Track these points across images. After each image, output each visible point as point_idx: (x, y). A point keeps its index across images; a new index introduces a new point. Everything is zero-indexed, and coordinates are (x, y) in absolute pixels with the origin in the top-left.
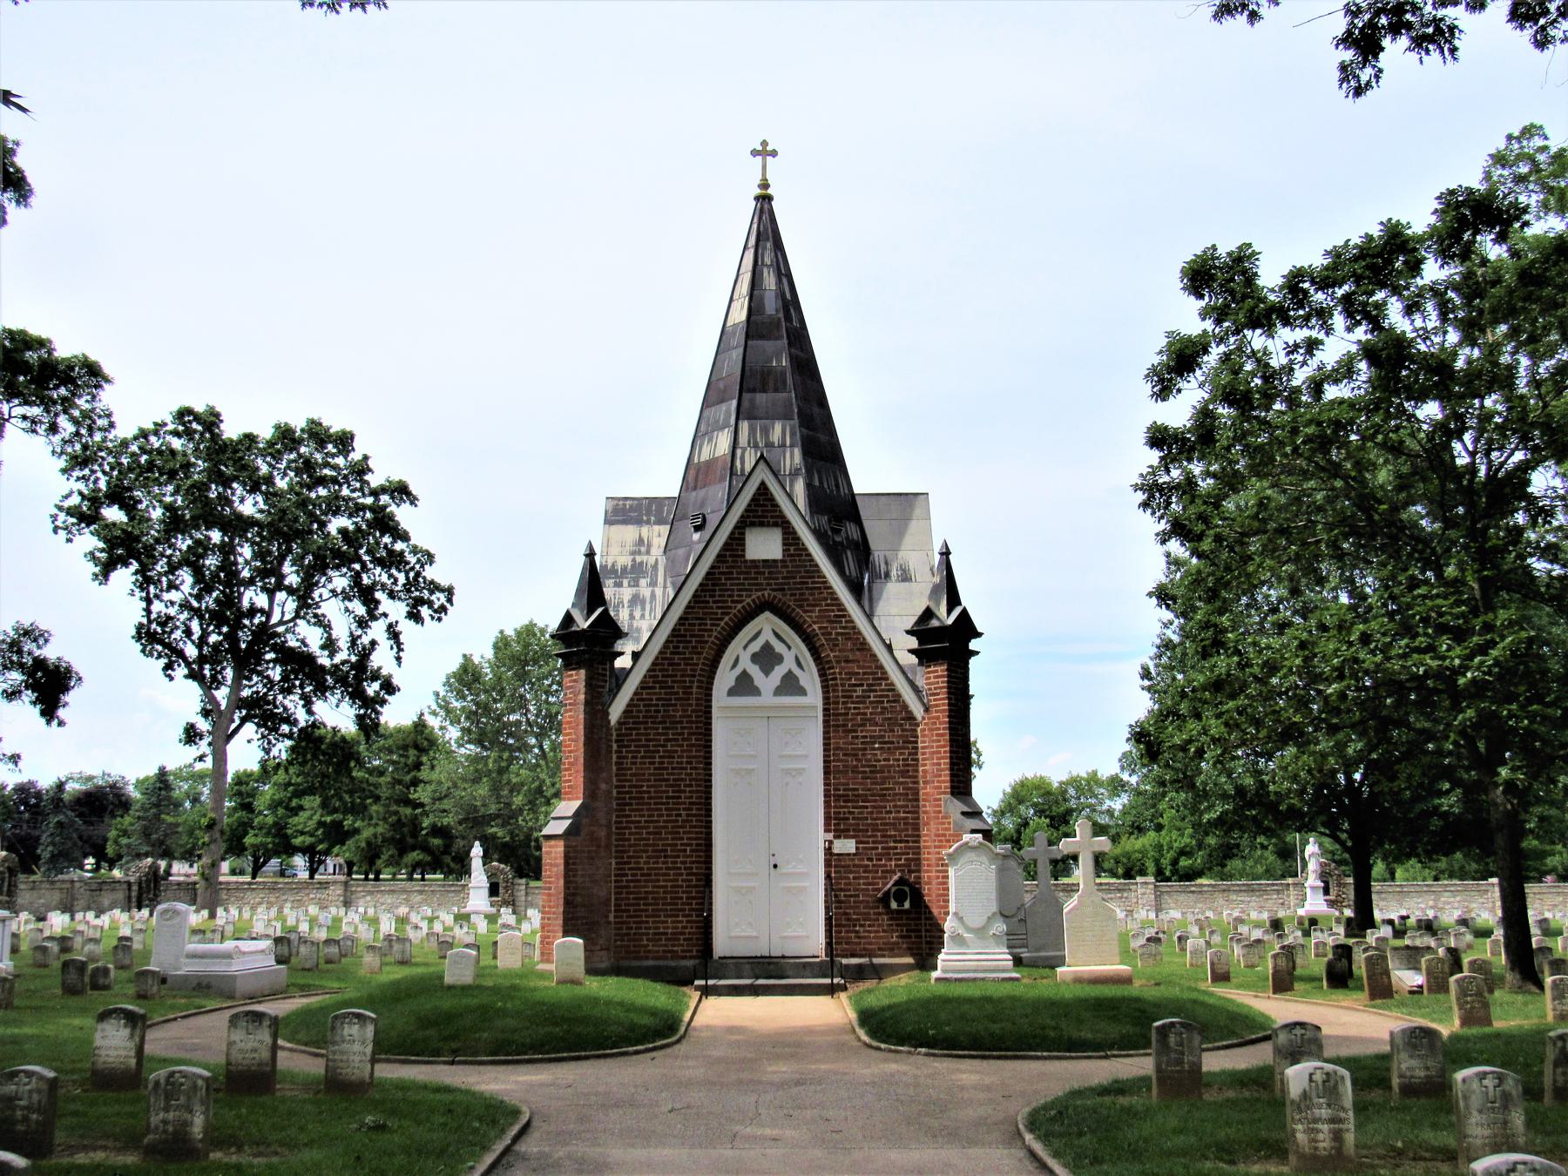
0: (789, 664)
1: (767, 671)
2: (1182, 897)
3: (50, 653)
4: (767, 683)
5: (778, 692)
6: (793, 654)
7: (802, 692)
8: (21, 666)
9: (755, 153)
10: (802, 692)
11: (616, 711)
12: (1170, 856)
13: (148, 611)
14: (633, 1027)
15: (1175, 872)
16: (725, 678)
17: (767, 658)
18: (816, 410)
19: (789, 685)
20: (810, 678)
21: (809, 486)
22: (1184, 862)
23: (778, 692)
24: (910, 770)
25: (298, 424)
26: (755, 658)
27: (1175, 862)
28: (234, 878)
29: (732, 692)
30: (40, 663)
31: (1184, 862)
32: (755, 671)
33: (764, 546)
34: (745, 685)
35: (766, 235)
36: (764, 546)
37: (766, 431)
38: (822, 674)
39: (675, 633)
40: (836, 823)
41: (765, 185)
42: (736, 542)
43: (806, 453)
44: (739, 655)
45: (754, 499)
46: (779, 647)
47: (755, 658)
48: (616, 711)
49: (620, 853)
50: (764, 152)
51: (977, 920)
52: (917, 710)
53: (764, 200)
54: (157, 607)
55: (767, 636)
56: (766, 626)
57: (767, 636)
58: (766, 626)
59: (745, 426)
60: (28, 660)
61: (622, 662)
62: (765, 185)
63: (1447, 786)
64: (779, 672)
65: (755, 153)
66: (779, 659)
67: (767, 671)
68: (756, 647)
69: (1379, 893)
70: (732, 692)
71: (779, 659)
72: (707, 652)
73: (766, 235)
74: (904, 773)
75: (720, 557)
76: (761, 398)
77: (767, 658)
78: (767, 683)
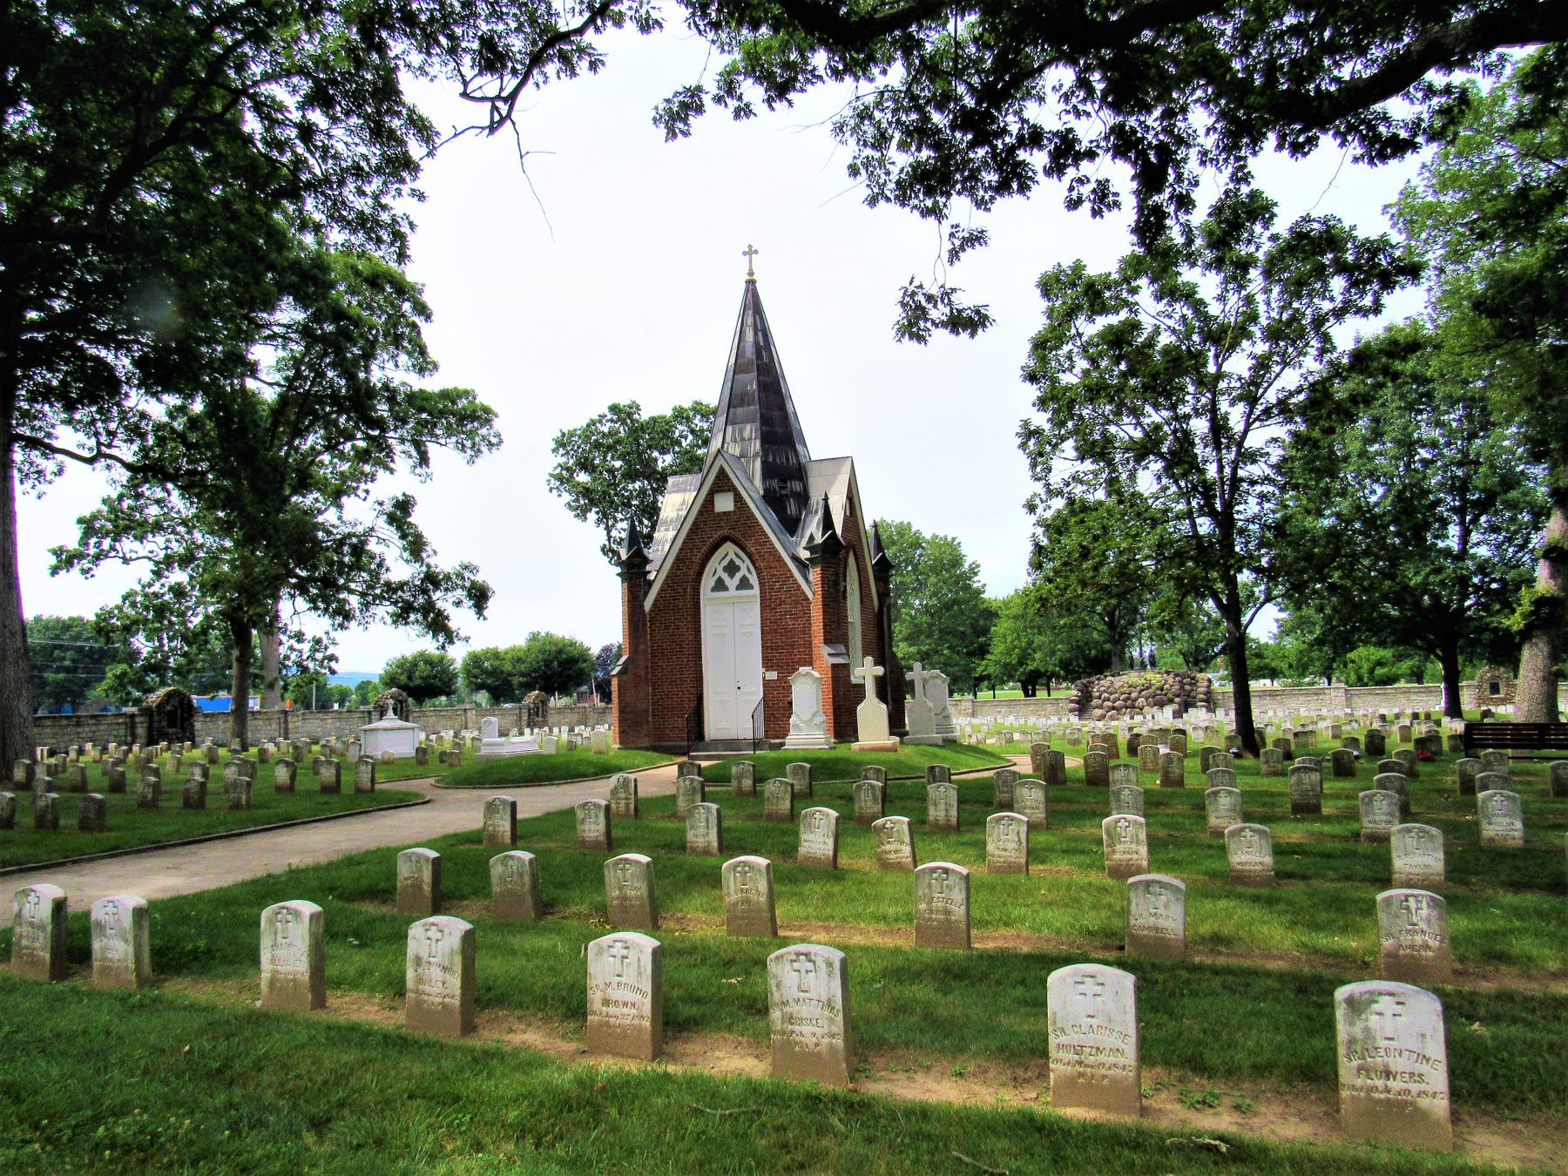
0: (743, 572)
1: (732, 576)
2: (1369, 698)
3: (479, 578)
4: (731, 583)
5: (738, 588)
6: (745, 565)
7: (751, 587)
8: (463, 587)
9: (745, 254)
10: (751, 587)
11: (648, 604)
12: (1366, 666)
13: (609, 537)
14: (582, 769)
15: (1372, 678)
16: (708, 581)
17: (732, 569)
18: (776, 413)
19: (744, 584)
20: (754, 579)
21: (764, 463)
22: (1379, 671)
23: (738, 588)
24: (807, 630)
25: (687, 404)
26: (725, 569)
27: (1371, 671)
28: (615, 696)
29: (714, 589)
30: (474, 585)
31: (1379, 671)
32: (725, 576)
33: (724, 504)
34: (720, 586)
35: (753, 305)
36: (724, 504)
37: (741, 432)
38: (759, 575)
39: (678, 558)
40: (768, 664)
41: (751, 274)
42: (709, 502)
43: (763, 443)
44: (715, 568)
45: (717, 477)
46: (738, 562)
47: (725, 569)
48: (648, 604)
49: (654, 684)
50: (750, 252)
51: (807, 717)
52: (810, 596)
53: (751, 283)
54: (614, 533)
55: (732, 556)
56: (729, 549)
57: (732, 556)
58: (729, 549)
59: (730, 429)
60: (468, 584)
61: (651, 577)
62: (751, 274)
63: (1498, 607)
64: (739, 576)
65: (745, 254)
66: (738, 569)
67: (732, 576)
68: (725, 563)
69: (1264, 694)
70: (714, 589)
71: (738, 569)
72: (696, 568)
73: (753, 305)
74: (804, 632)
75: (700, 512)
76: (740, 410)
77: (732, 569)
78: (731, 583)
